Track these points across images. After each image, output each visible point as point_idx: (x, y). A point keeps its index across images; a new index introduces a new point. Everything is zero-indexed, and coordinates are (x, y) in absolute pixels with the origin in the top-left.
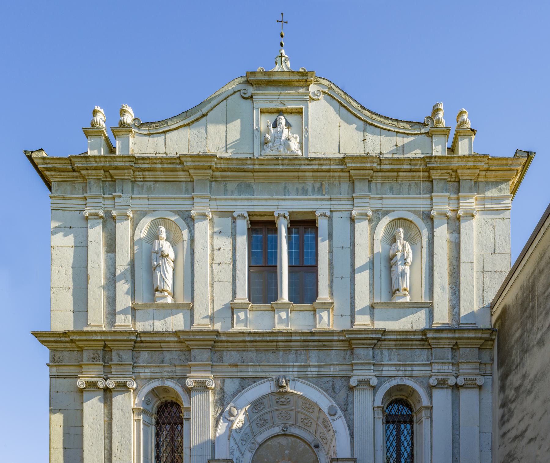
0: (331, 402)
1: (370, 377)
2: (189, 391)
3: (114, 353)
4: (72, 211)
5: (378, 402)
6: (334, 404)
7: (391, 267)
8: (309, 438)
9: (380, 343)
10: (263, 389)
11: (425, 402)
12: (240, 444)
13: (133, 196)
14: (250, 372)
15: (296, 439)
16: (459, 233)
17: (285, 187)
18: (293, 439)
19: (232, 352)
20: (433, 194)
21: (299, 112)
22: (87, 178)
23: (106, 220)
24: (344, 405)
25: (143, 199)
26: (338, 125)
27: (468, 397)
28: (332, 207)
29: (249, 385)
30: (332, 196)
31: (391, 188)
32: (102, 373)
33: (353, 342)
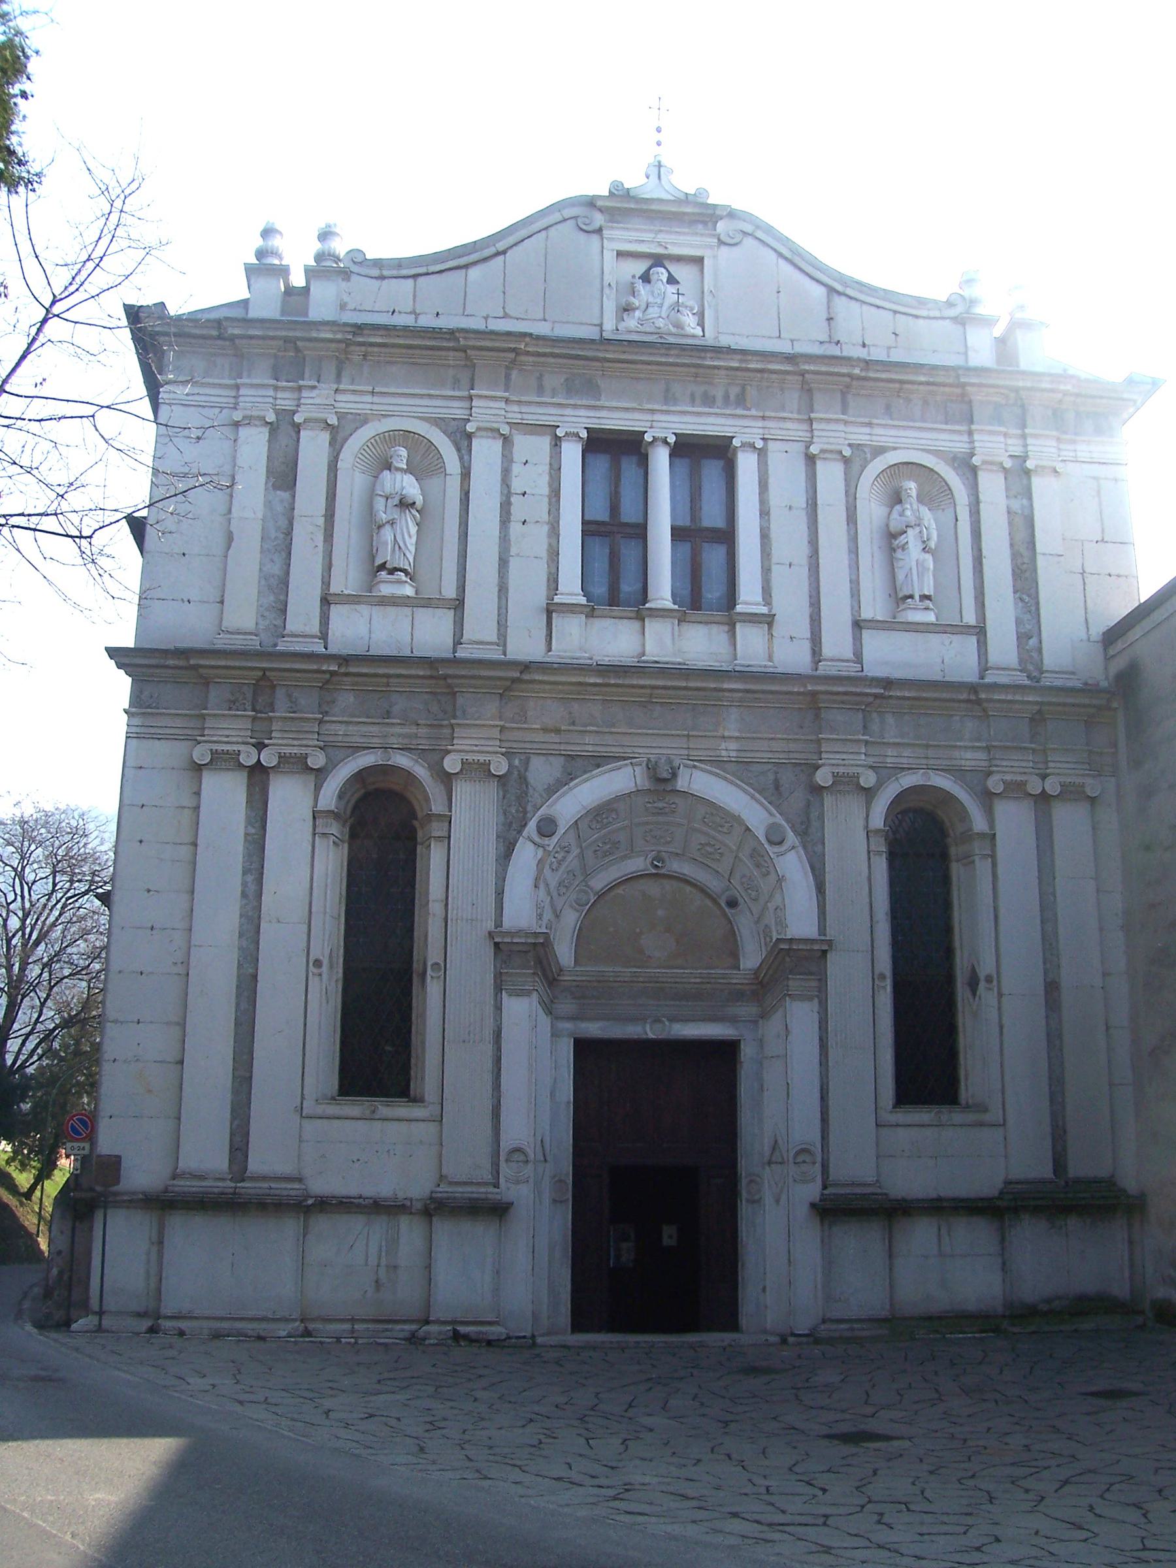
0: (771, 814)
1: (860, 770)
2: (447, 779)
3: (280, 693)
4: (204, 407)
5: (878, 820)
6: (779, 819)
7: (894, 550)
8: (714, 884)
9: (878, 701)
10: (618, 781)
11: (979, 823)
12: (555, 894)
13: (342, 387)
14: (588, 744)
15: (682, 885)
16: (1030, 498)
17: (667, 390)
18: (675, 883)
19: (549, 702)
20: (973, 427)
21: (699, 261)
22: (245, 350)
23: (278, 428)
24: (802, 823)
25: (362, 393)
26: (776, 289)
27: (1069, 820)
28: (766, 431)
29: (585, 772)
30: (767, 414)
31: (888, 407)
32: (249, 733)
33: (822, 697)
